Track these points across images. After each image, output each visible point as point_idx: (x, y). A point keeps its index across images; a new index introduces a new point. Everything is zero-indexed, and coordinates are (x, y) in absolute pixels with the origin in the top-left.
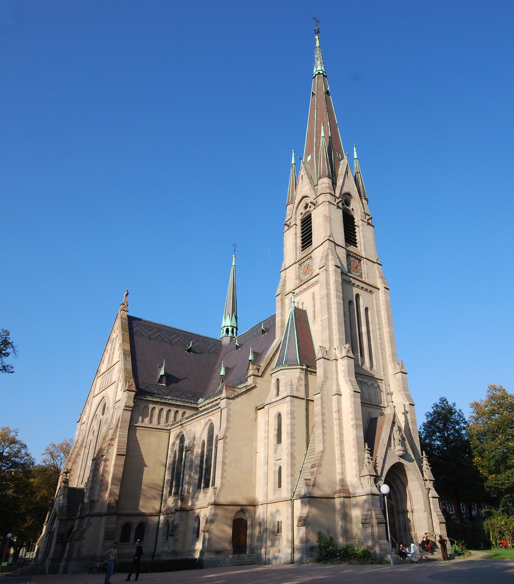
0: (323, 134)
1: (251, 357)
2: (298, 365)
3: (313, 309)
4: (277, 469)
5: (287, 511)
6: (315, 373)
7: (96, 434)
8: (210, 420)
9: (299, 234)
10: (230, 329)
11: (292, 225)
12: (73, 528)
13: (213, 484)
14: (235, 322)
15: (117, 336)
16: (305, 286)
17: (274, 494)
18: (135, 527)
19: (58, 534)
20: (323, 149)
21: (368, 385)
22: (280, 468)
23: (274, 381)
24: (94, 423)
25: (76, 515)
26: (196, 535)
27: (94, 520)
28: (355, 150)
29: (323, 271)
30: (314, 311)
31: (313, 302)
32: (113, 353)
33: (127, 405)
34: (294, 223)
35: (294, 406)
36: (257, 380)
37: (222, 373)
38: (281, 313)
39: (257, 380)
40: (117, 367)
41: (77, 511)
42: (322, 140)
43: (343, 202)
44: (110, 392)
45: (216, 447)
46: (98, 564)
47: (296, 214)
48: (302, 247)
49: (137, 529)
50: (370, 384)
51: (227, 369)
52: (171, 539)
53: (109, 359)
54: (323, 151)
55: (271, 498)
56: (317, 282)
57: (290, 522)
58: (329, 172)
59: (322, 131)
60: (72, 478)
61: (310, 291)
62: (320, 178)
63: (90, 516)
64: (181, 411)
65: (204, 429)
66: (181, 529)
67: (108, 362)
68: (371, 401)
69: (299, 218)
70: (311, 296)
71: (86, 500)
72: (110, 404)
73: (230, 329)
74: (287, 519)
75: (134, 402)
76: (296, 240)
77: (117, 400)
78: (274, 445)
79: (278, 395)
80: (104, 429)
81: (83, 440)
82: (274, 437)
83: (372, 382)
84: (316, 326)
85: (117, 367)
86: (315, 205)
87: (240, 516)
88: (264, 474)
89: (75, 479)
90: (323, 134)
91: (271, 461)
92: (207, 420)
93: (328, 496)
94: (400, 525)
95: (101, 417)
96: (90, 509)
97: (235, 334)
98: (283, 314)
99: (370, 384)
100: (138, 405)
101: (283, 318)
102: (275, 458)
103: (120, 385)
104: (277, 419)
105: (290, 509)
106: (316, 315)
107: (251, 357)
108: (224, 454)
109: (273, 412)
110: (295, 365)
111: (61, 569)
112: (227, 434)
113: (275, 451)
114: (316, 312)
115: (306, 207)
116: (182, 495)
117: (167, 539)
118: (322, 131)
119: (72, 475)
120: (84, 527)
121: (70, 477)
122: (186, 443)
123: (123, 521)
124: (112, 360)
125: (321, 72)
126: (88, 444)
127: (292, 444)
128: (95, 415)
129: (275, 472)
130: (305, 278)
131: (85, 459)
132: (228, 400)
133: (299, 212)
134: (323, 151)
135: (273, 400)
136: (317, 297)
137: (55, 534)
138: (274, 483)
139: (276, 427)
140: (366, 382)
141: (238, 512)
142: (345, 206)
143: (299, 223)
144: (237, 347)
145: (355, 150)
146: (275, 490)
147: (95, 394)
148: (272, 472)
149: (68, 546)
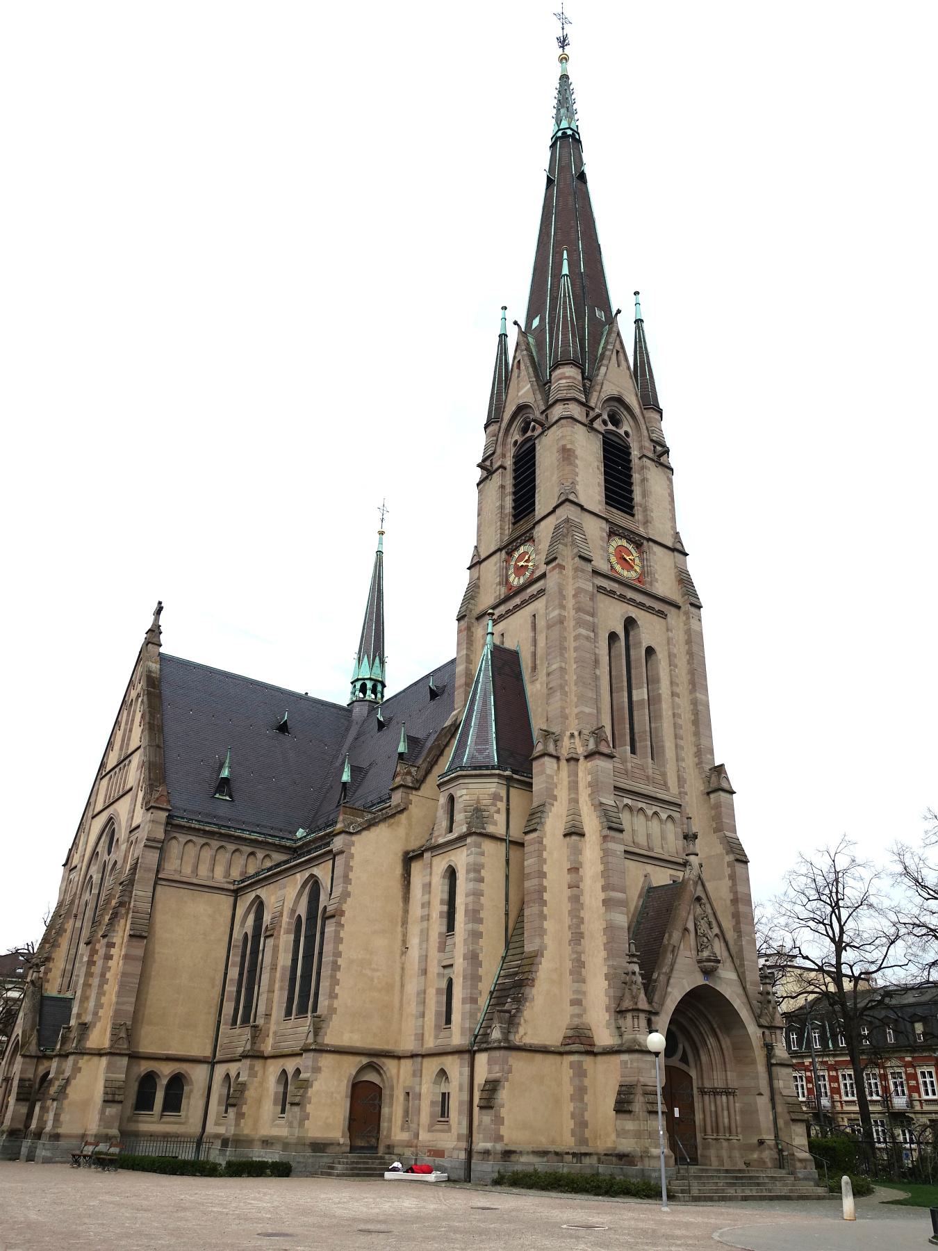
0: (565, 270)
1: (402, 748)
2: (493, 768)
3: (532, 649)
4: (444, 985)
5: (461, 1074)
6: (530, 785)
7: (95, 891)
8: (312, 876)
9: (509, 489)
10: (369, 685)
11: (495, 466)
12: (48, 1073)
13: (315, 1009)
14: (379, 671)
15: (138, 696)
16: (517, 601)
17: (436, 1037)
18: (165, 1082)
19: (21, 1080)
20: (565, 302)
21: (646, 816)
22: (450, 982)
23: (443, 800)
24: (93, 869)
25: (53, 1050)
26: (279, 1108)
27: (83, 1062)
28: (565, 256)
29: (554, 568)
30: (534, 654)
31: (532, 634)
32: (131, 731)
33: (153, 836)
34: (499, 464)
35: (483, 854)
36: (411, 797)
37: (346, 777)
38: (467, 655)
39: (411, 797)
40: (136, 760)
41: (56, 1043)
42: (566, 283)
43: (605, 417)
44: (122, 808)
45: (323, 933)
46: (89, 1150)
47: (504, 444)
48: (515, 516)
49: (169, 1086)
50: (650, 813)
51: (355, 770)
52: (231, 1111)
53: (123, 741)
54: (565, 308)
55: (430, 1044)
56: (542, 592)
57: (466, 1097)
58: (575, 352)
59: (565, 263)
60: (50, 976)
61: (524, 615)
62: (556, 366)
63: (82, 1053)
64: (260, 855)
65: (300, 894)
66: (250, 1093)
67: (121, 749)
68: (650, 849)
69: (511, 452)
70: (529, 620)
71: (73, 1022)
72: (122, 833)
73: (369, 685)
74: (461, 1089)
75: (166, 831)
76: (502, 499)
77: (134, 825)
78: (440, 934)
79: (451, 831)
80: (109, 881)
81: (72, 902)
82: (441, 917)
83: (655, 809)
84: (538, 686)
85: (136, 760)
86: (542, 425)
87: (371, 1077)
88: (418, 994)
89: (55, 979)
90: (565, 270)
91: (434, 969)
92: (253, 895)
93: (414, 1185)
94: (704, 1120)
95: (106, 857)
96: (79, 1041)
97: (379, 695)
98: (472, 657)
99: (650, 813)
100: (175, 838)
101: (471, 667)
102: (440, 961)
103: (141, 795)
104: (447, 881)
105: (466, 1070)
106: (538, 662)
107: (402, 748)
108: (336, 948)
109: (440, 865)
110: (487, 768)
111: (24, 1151)
112: (345, 907)
113: (442, 948)
114: (538, 656)
115: (525, 430)
116: (255, 1027)
117: (226, 1112)
118: (565, 263)
119: (50, 970)
120: (67, 1074)
121: (46, 973)
122: (267, 918)
123: (145, 1067)
124: (128, 745)
125: (569, 132)
126: (82, 909)
127: (476, 935)
128: (95, 854)
129: (439, 991)
130: (516, 581)
131: (75, 941)
132: (347, 837)
133: (511, 440)
134: (565, 308)
135: (441, 840)
136: (541, 623)
137: (15, 1083)
138: (438, 1014)
139: (446, 897)
140: (641, 809)
141: (362, 1069)
142: (610, 427)
143: (509, 462)
144: (381, 725)
145: (565, 256)
146: (437, 1027)
147: (97, 811)
148: (434, 991)
149: (37, 1109)
